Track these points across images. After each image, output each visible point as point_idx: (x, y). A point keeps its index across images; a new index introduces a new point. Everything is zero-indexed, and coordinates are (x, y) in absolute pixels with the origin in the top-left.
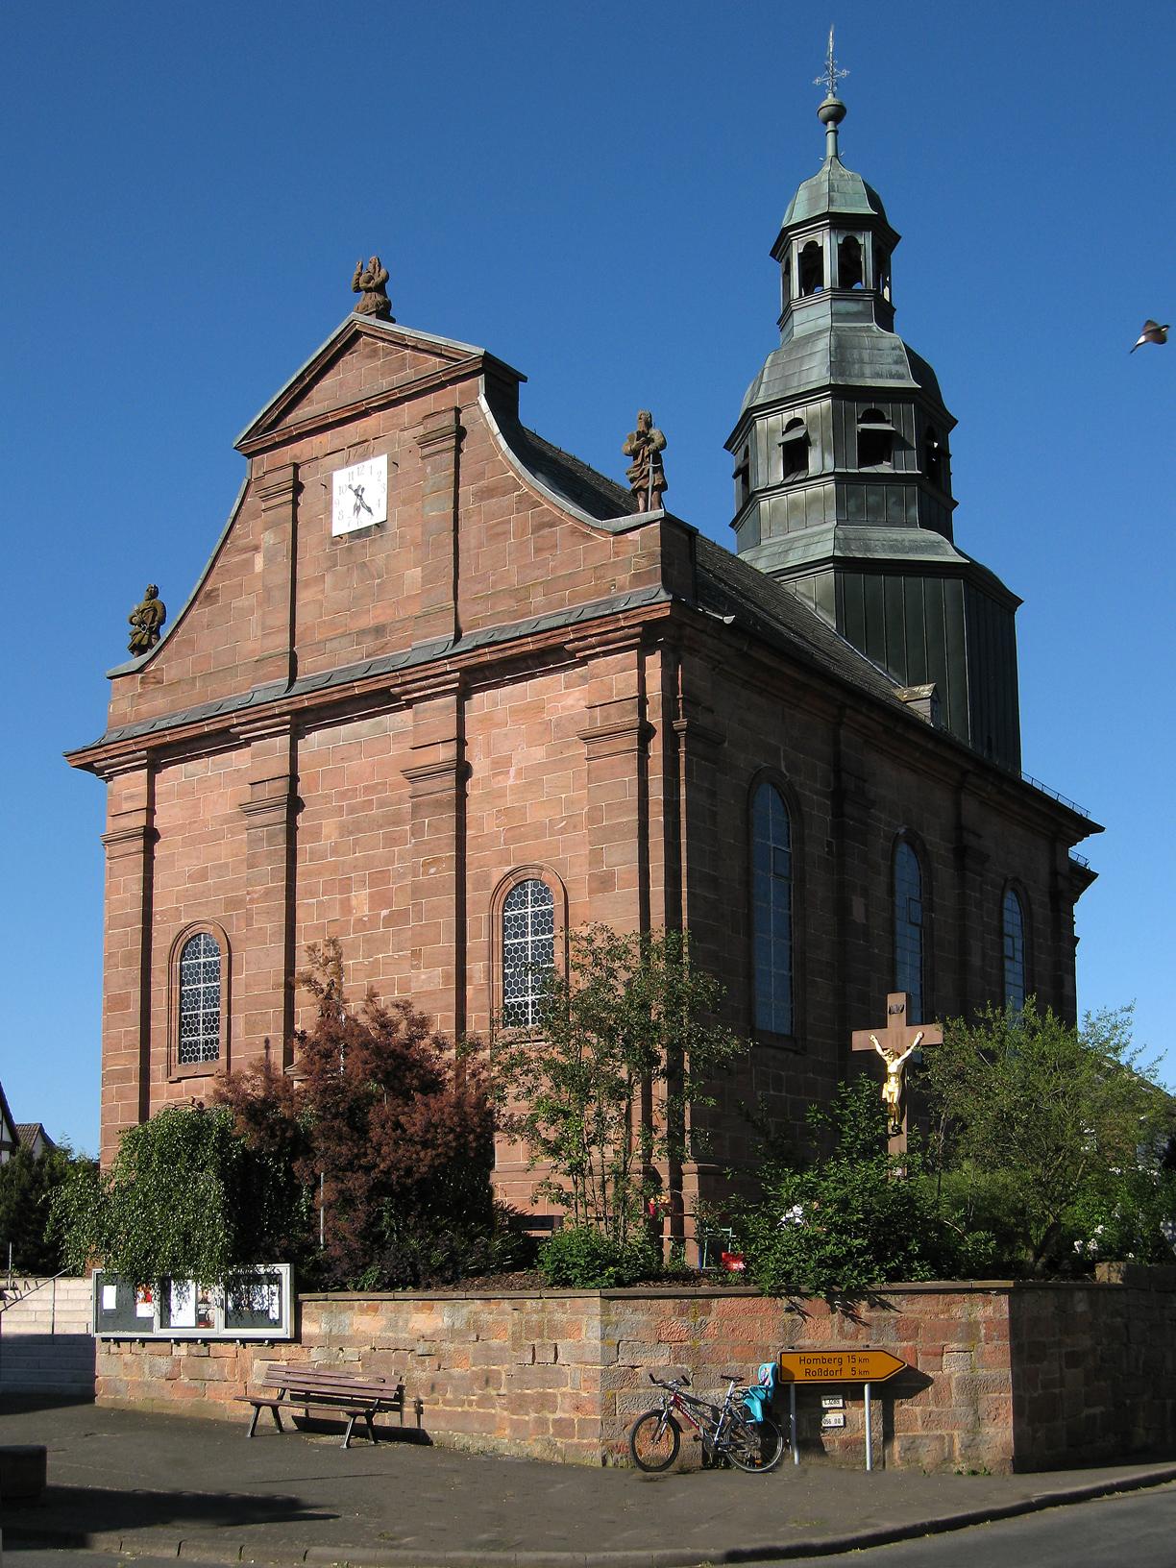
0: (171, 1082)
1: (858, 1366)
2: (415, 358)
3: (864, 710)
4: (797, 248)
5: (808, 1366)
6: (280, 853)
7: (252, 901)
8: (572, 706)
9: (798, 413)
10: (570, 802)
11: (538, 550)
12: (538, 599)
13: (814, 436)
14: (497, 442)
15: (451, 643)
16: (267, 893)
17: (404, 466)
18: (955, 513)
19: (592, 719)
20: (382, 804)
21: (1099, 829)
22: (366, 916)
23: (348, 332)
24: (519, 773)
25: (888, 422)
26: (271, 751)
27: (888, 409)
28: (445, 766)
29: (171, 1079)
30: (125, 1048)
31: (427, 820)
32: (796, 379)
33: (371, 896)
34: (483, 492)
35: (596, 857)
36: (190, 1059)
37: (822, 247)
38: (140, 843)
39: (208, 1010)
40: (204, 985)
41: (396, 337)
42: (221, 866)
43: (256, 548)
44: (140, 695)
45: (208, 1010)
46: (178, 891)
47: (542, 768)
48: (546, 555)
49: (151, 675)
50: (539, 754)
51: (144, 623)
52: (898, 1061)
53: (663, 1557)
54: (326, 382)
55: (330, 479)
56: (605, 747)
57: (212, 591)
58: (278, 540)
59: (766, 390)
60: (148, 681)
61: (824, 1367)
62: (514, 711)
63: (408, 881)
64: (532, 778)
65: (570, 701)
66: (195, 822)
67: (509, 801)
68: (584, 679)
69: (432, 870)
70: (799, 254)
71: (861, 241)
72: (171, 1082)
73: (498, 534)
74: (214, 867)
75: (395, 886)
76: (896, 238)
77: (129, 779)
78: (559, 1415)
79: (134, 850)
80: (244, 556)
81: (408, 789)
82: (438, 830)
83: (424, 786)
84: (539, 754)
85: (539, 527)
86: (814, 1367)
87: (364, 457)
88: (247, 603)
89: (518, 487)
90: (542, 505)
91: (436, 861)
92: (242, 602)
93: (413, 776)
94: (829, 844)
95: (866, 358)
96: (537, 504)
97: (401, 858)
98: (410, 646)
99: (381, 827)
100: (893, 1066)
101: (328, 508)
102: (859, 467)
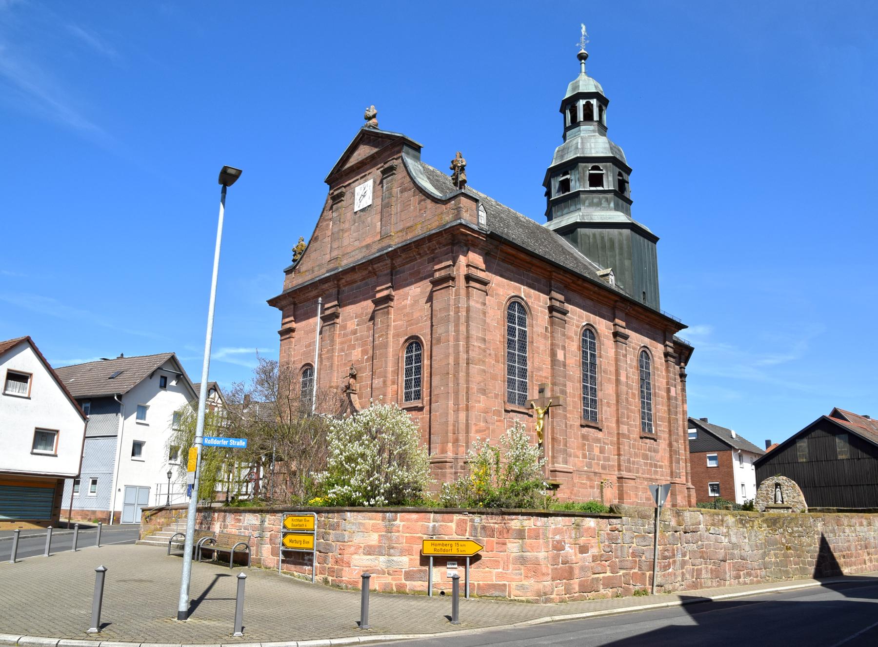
1: (461, 548)
3: (561, 273)
5: (435, 547)
11: (420, 210)
27: (601, 165)
33: (362, 351)
44: (293, 278)
53: (430, 637)
55: (354, 191)
61: (443, 548)
67: (408, 310)
71: (592, 103)
78: (330, 565)
86: (438, 548)
87: (366, 181)
94: (546, 328)
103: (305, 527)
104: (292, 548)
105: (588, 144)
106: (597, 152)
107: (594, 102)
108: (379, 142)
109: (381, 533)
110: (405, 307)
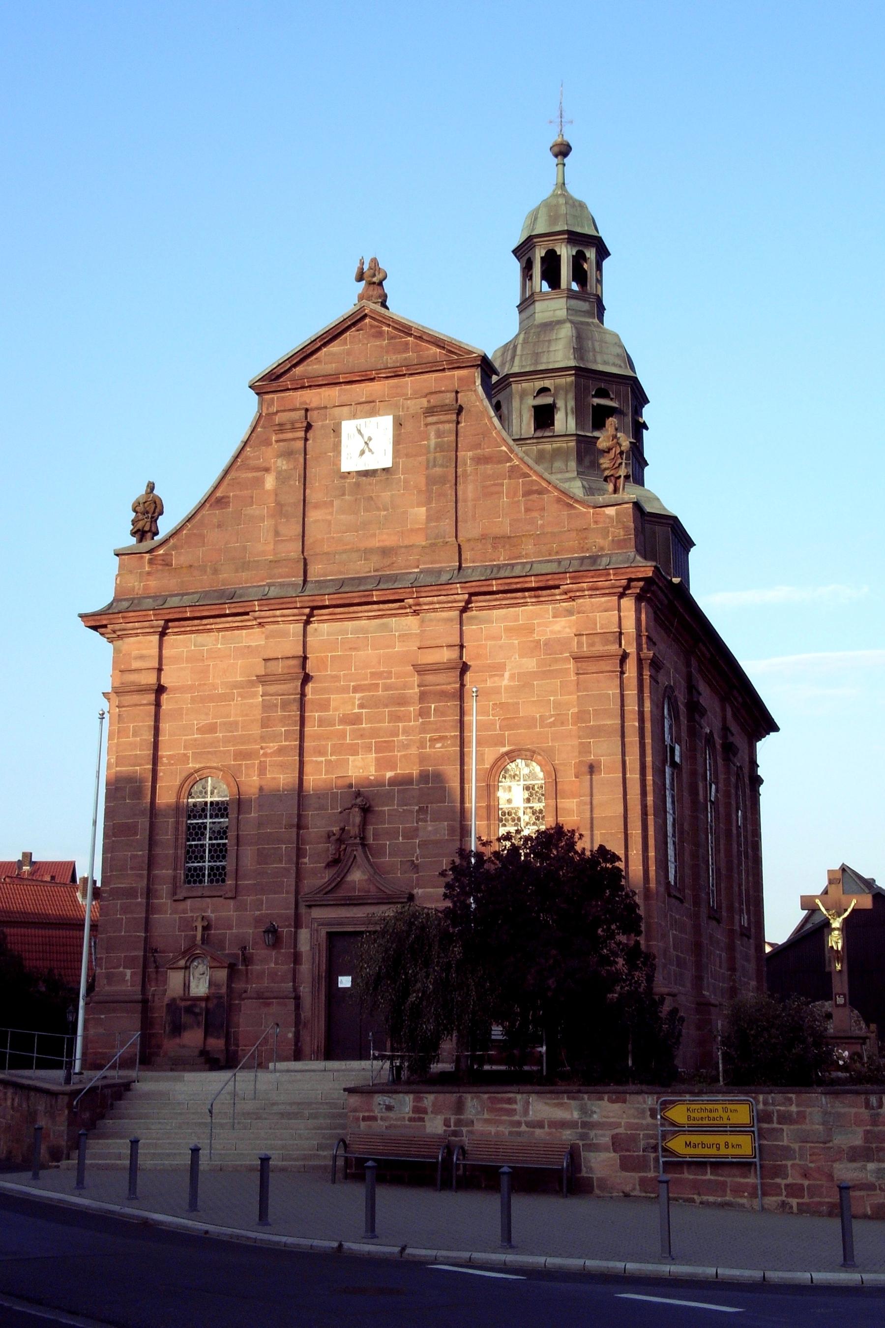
0: (175, 901)
2: (417, 345)
4: (539, 253)
6: (294, 718)
7: (265, 755)
8: (559, 632)
9: (547, 383)
10: (558, 705)
11: (527, 510)
12: (529, 547)
13: (560, 404)
14: (492, 423)
15: (456, 572)
16: (281, 751)
17: (409, 427)
18: (646, 470)
19: (580, 644)
20: (387, 688)
21: (82, 616)
22: (372, 775)
23: (358, 314)
24: (512, 677)
25: (612, 399)
26: (284, 634)
27: (612, 390)
28: (453, 665)
29: (176, 898)
30: (132, 868)
31: (433, 706)
32: (545, 357)
33: (377, 759)
34: (479, 459)
35: (584, 749)
36: (195, 882)
37: (560, 256)
38: (152, 697)
39: (214, 842)
40: (211, 820)
41: (403, 326)
42: (231, 723)
43: (267, 470)
44: (149, 573)
45: (214, 842)
46: (186, 740)
47: (534, 675)
48: (535, 514)
49: (159, 558)
50: (530, 664)
51: (147, 513)
52: (841, 919)
54: (334, 348)
56: (592, 667)
57: (223, 498)
58: (291, 466)
59: (521, 360)
60: (156, 562)
62: (508, 630)
63: (414, 751)
64: (525, 682)
65: (557, 628)
66: (205, 684)
68: (570, 613)
69: (439, 745)
70: (542, 258)
71: (588, 255)
72: (175, 901)
73: (492, 494)
74: (225, 724)
75: (399, 754)
76: (608, 254)
77: (140, 642)
79: (145, 702)
80: (255, 474)
81: (416, 679)
82: (443, 714)
83: (430, 678)
84: (530, 664)
85: (527, 493)
88: (258, 512)
89: (510, 460)
90: (531, 476)
91: (441, 739)
92: (254, 510)
93: (421, 670)
95: (598, 349)
96: (526, 475)
97: (406, 732)
98: (418, 567)
99: (386, 706)
100: (836, 923)
101: (337, 447)
102: (592, 432)
103: (726, 1121)
104: (691, 1156)
105: (590, 343)
106: (605, 363)
107: (591, 254)
108: (407, 343)
109: (865, 1128)
110: (497, 691)
